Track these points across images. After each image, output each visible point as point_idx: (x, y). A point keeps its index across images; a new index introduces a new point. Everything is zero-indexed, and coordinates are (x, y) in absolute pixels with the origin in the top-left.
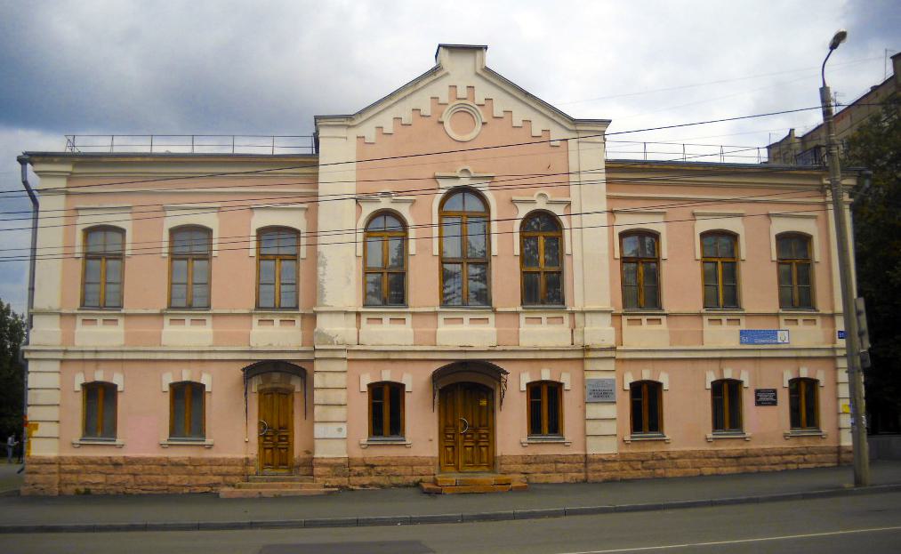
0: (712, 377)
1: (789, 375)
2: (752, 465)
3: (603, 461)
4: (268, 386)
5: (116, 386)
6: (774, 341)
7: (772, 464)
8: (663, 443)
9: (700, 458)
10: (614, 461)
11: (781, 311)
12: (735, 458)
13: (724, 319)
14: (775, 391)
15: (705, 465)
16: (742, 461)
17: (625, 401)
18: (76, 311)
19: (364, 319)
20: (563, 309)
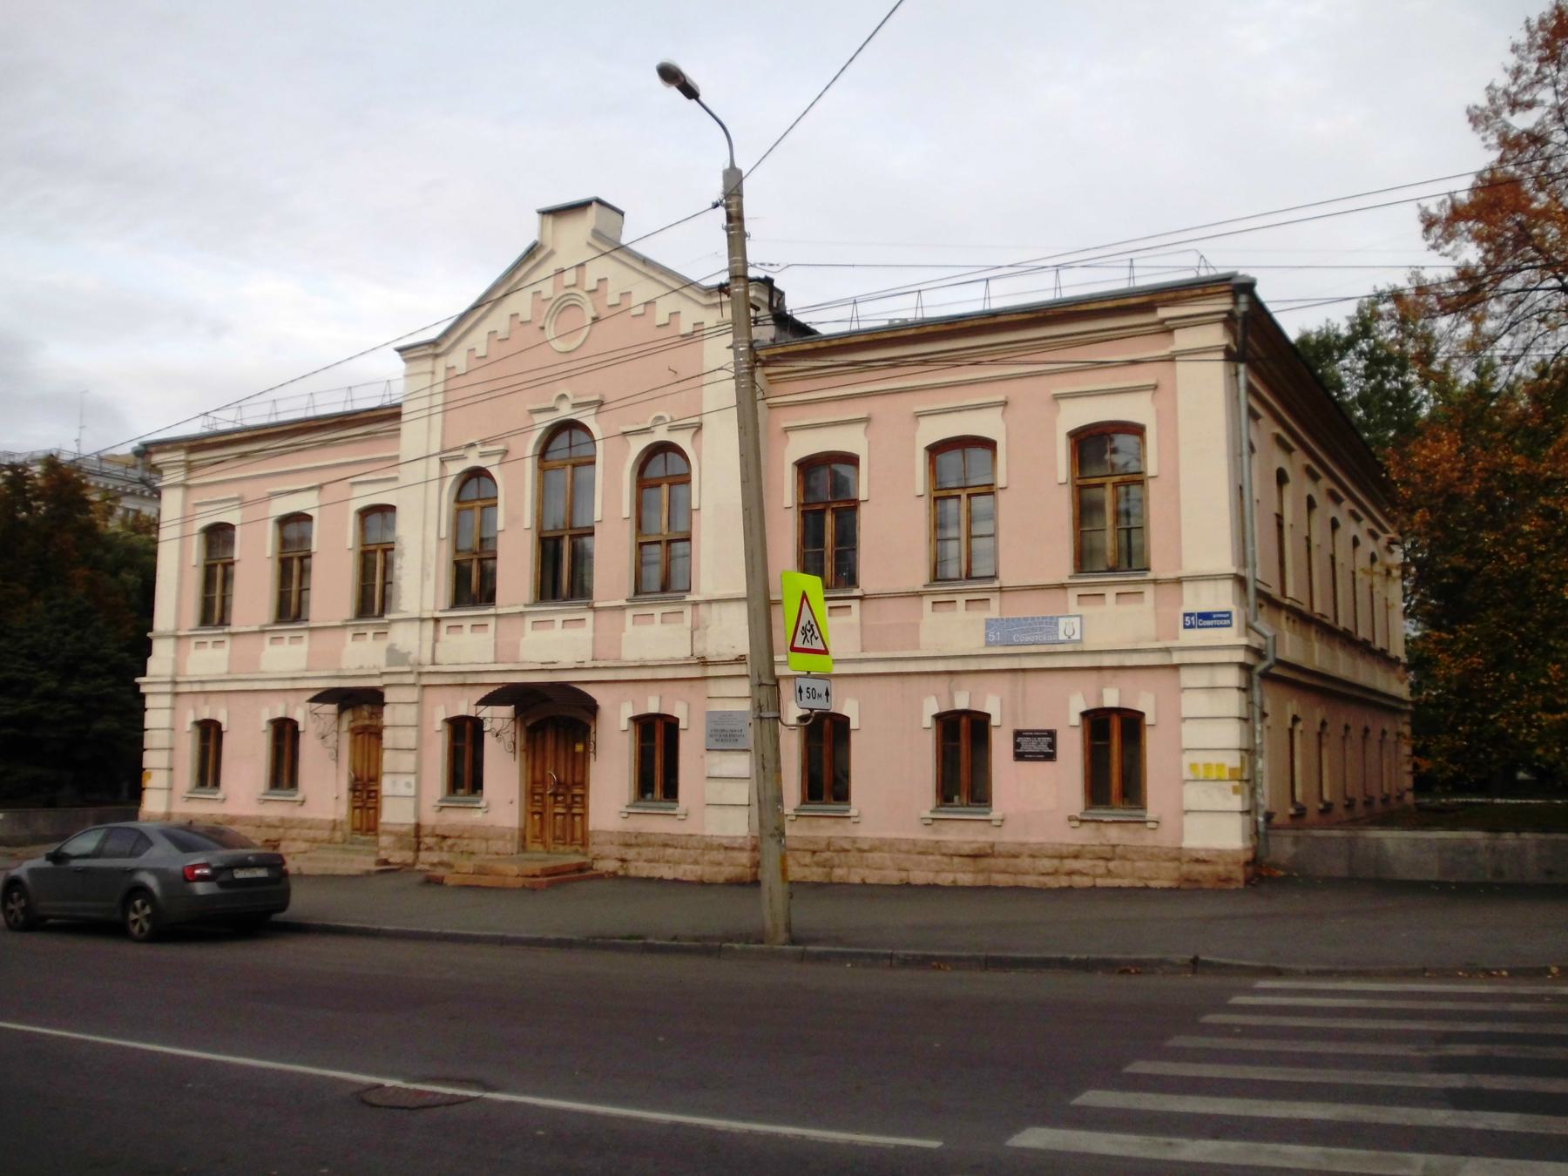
0: (932, 707)
1: (1078, 704)
2: (1004, 872)
4: (360, 723)
5: (988, 716)
6: (1051, 639)
7: (1043, 874)
9: (908, 852)
10: (741, 849)
12: (968, 856)
14: (1052, 734)
17: (1072, 747)
18: (1065, 580)
19: (443, 626)
20: (680, 601)
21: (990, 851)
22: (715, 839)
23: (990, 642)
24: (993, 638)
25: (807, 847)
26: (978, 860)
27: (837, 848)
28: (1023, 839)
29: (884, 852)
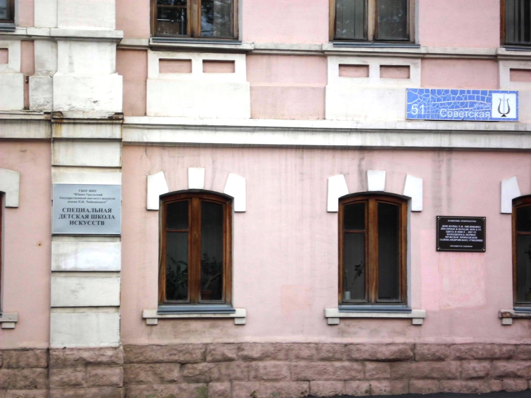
3: (87, 364)
6: (483, 116)
7: (472, 378)
8: (229, 323)
9: (310, 358)
10: (111, 364)
11: (502, 51)
13: (374, 64)
14: (481, 222)
15: (322, 373)
16: (403, 367)
21: (411, 354)
22: (68, 352)
23: (413, 116)
24: (415, 110)
25: (176, 358)
26: (396, 364)
27: (219, 357)
28: (449, 340)
29: (280, 360)
